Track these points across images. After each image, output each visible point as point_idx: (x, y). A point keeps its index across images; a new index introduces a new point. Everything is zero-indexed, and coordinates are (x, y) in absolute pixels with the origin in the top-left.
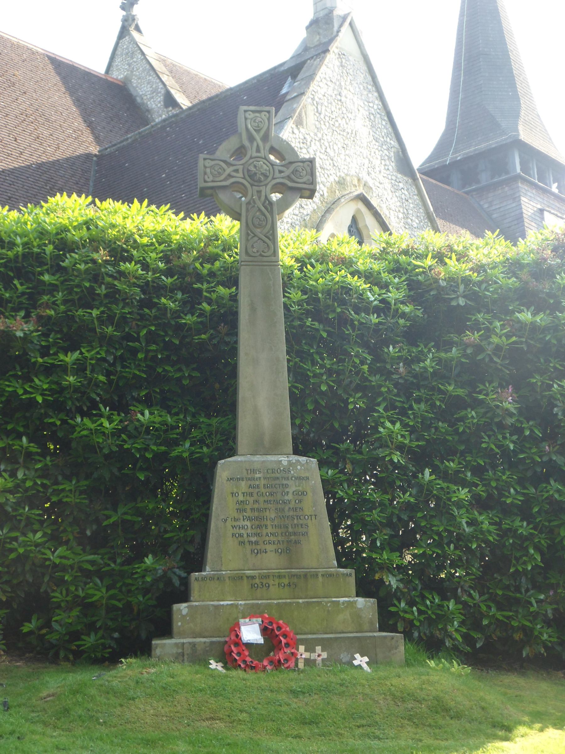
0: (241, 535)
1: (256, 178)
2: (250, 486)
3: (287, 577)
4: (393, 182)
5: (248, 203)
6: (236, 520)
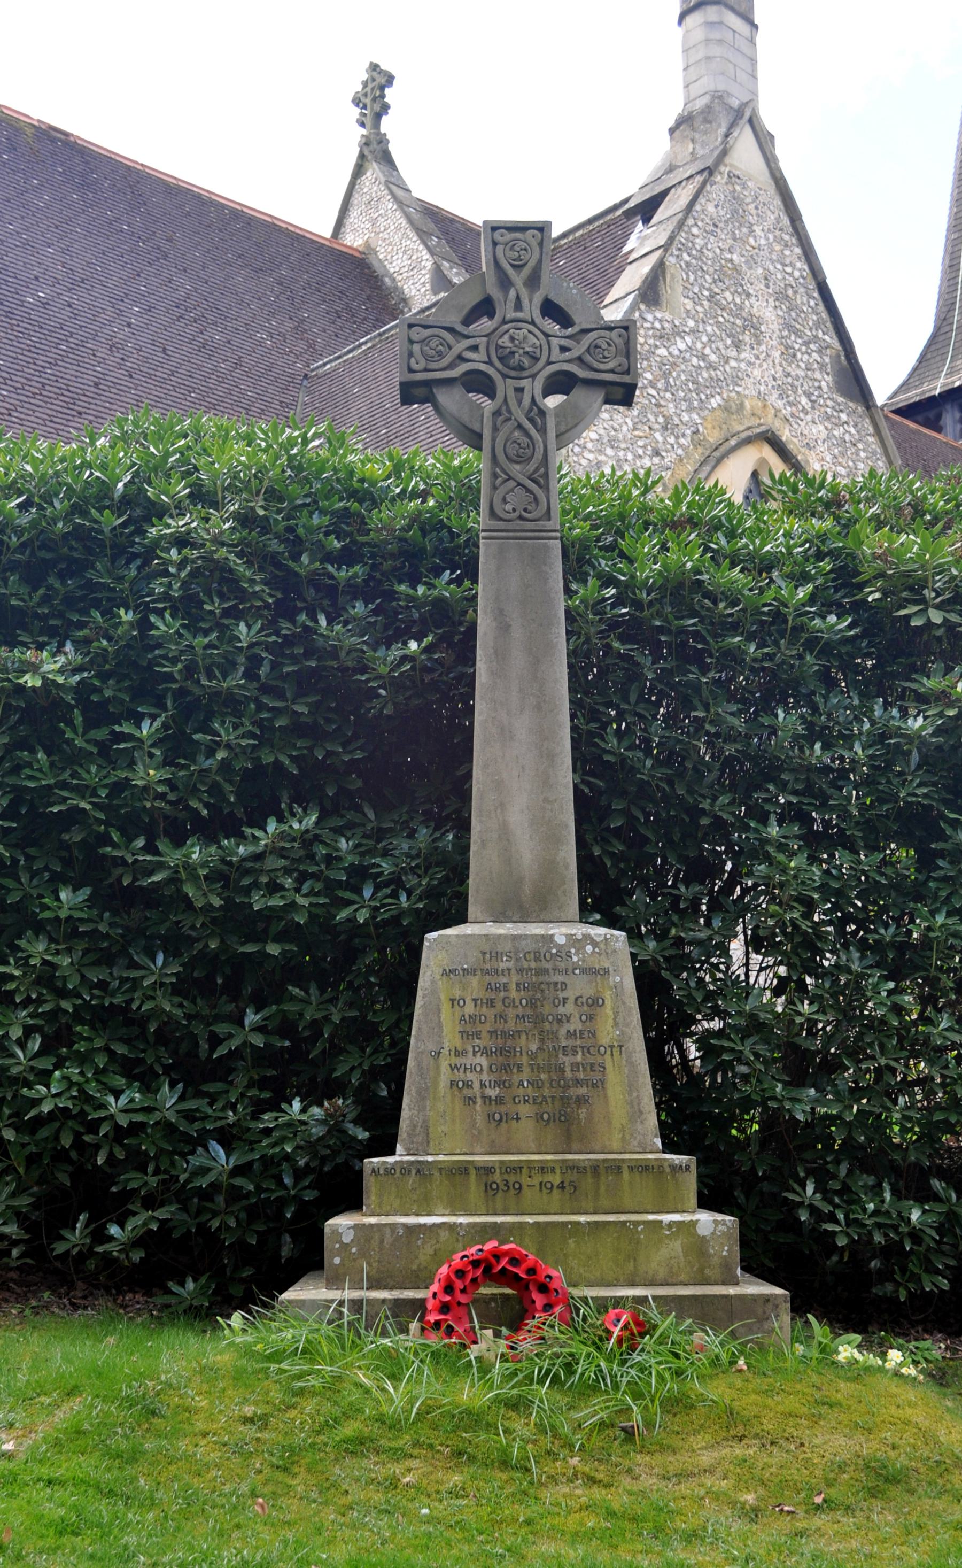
0: (468, 1085)
1: (513, 362)
2: (489, 987)
3: (558, 1171)
4: (829, 410)
5: (496, 413)
6: (458, 1053)
